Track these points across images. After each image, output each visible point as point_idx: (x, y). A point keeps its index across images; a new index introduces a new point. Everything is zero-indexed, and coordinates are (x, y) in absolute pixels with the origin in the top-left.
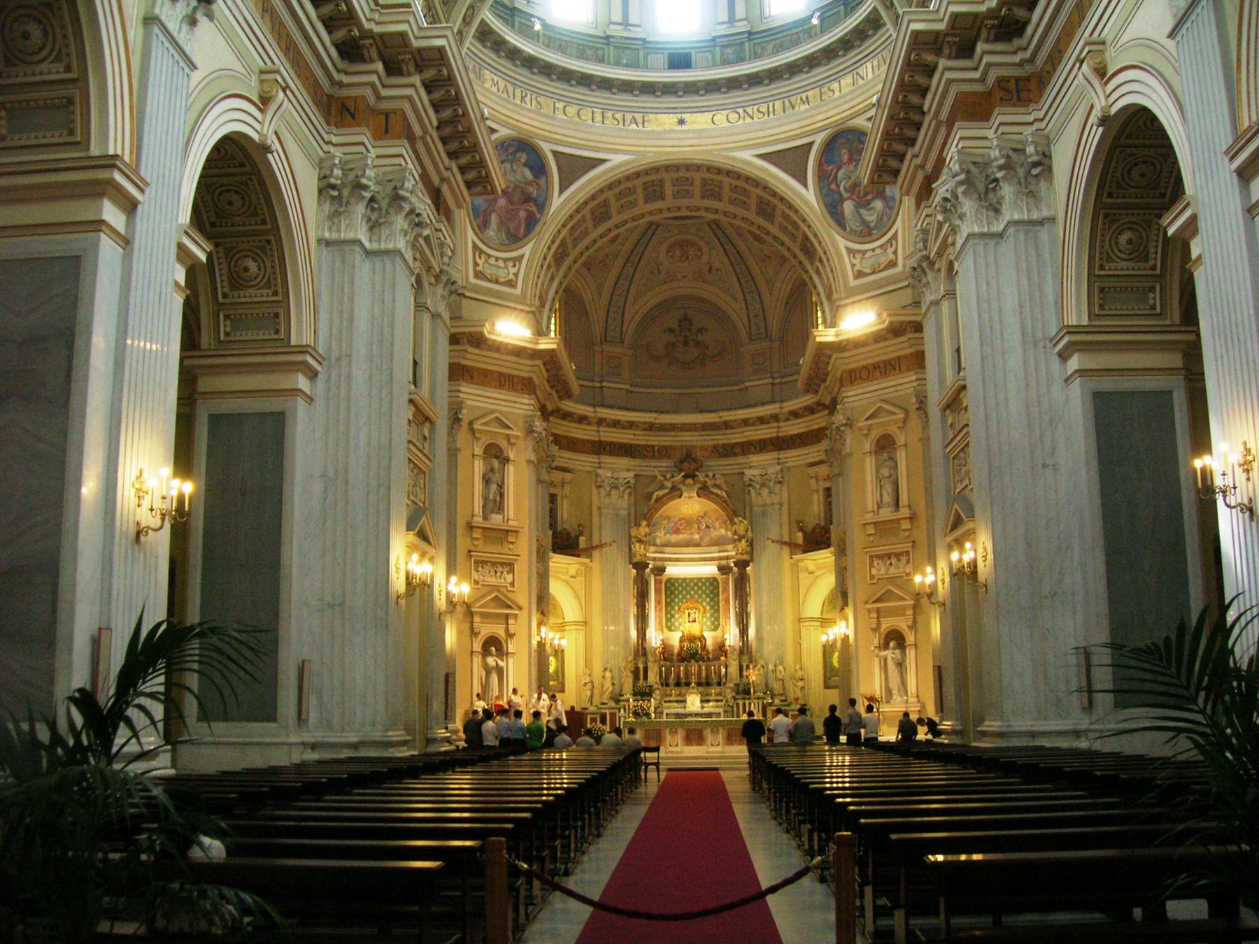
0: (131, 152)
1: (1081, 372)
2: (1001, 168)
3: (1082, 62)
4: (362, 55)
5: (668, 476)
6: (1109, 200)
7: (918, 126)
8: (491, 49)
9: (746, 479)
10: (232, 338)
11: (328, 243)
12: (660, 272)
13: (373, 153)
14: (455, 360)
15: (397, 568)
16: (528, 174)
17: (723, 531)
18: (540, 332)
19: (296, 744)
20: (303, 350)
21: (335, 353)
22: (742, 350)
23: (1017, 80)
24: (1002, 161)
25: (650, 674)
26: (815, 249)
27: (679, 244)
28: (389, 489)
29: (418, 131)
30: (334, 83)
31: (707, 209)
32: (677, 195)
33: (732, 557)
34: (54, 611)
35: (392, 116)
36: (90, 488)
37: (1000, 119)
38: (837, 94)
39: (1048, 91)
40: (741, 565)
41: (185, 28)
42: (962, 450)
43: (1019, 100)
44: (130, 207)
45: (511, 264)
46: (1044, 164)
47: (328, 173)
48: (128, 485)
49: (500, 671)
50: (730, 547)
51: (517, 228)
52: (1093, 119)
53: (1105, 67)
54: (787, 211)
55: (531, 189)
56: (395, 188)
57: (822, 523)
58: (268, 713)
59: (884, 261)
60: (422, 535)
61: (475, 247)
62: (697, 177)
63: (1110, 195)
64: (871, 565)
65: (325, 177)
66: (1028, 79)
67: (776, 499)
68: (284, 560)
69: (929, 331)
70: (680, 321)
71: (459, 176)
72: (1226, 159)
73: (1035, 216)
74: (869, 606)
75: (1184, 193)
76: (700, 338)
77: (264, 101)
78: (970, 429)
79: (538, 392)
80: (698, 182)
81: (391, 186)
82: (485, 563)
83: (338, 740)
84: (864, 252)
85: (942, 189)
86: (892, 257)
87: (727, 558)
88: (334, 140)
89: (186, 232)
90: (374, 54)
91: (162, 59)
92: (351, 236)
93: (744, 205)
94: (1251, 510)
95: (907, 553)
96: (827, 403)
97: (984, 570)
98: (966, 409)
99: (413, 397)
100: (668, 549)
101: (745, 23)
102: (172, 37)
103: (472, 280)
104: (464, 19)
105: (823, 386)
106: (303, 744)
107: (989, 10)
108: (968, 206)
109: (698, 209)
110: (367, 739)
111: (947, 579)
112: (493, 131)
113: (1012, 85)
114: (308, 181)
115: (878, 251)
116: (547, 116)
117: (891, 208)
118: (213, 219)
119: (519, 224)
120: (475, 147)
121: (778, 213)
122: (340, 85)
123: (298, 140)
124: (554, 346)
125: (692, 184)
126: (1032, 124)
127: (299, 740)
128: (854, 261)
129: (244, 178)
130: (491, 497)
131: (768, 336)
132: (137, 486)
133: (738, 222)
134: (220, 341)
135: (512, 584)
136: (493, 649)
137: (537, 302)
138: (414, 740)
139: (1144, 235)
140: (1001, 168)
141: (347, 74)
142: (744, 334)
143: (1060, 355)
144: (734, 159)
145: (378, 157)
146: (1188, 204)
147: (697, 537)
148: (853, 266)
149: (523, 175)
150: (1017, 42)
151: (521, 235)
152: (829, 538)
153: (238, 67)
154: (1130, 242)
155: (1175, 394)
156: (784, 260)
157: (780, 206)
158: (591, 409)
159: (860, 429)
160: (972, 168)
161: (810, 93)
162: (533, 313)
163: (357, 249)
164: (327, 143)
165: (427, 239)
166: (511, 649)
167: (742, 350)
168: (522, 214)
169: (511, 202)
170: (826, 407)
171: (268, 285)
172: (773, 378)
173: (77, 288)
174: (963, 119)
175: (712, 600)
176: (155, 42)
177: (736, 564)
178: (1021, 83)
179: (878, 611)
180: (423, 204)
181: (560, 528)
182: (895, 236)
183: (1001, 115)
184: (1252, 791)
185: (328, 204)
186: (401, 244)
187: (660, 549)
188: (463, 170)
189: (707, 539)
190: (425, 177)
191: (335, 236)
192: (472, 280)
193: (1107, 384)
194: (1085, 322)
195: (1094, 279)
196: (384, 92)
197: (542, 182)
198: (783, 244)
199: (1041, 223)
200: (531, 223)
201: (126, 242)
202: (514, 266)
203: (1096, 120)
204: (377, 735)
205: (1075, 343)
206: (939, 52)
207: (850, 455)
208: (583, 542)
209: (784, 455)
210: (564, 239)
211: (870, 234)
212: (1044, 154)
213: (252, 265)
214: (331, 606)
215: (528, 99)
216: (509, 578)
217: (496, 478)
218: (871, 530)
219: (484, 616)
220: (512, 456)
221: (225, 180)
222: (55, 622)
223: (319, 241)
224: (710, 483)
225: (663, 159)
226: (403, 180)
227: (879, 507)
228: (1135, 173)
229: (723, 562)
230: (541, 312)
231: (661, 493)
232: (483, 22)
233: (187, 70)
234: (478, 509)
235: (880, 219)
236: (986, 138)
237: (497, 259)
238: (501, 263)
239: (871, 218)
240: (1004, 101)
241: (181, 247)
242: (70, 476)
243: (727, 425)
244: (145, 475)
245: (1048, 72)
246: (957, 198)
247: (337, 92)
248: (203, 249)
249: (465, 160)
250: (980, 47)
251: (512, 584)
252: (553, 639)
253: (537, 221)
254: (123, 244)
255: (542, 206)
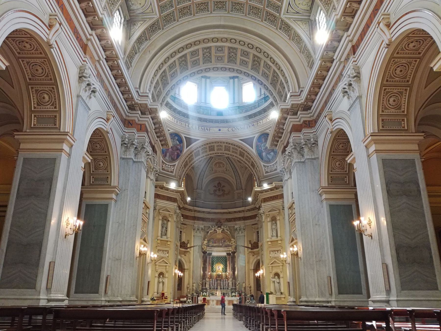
0: (72, 131)
1: (326, 199)
2: (304, 145)
3: (326, 117)
4: (135, 109)
5: (213, 227)
6: (333, 153)
7: (282, 133)
8: (169, 108)
9: (235, 228)
10: (94, 183)
11: (123, 159)
12: (213, 170)
13: (137, 135)
14: (156, 192)
15: (137, 249)
16: (178, 143)
17: (228, 243)
18: (180, 186)
19: (104, 300)
20: (115, 187)
21: (124, 189)
22: (235, 192)
23: (309, 121)
24: (304, 143)
25: (206, 285)
26: (255, 165)
27: (219, 163)
28: (136, 226)
29: (149, 130)
30: (126, 116)
31: (226, 154)
32: (218, 150)
33: (231, 251)
34: (40, 256)
35: (142, 126)
36: (53, 222)
37: (304, 131)
38: (262, 123)
39: (317, 124)
40: (234, 253)
41: (88, 99)
42: (294, 220)
43: (309, 126)
44: (71, 146)
45: (172, 167)
46: (316, 143)
47: (124, 140)
48: (64, 221)
49: (163, 283)
50: (230, 248)
51: (174, 157)
52: (329, 132)
53: (332, 118)
54: (248, 155)
55: (178, 147)
56: (143, 145)
57: (256, 242)
58: (96, 291)
59: (274, 169)
60: (145, 240)
61: (162, 162)
62: (224, 145)
63: (333, 152)
64: (270, 254)
65: (123, 141)
66: (312, 121)
67: (243, 234)
68: (105, 246)
69: (285, 188)
70: (218, 184)
71: (159, 142)
72: (362, 143)
73: (313, 157)
74: (269, 265)
75: (351, 151)
76: (223, 188)
77: (108, 120)
78: (296, 214)
79: (178, 202)
80: (224, 146)
81: (142, 144)
82: (161, 250)
83: (116, 299)
84: (268, 166)
85: (288, 149)
86: (275, 168)
87: (229, 251)
88: (126, 131)
89: (85, 154)
90: (138, 109)
91: (81, 109)
92: (129, 157)
93: (236, 153)
94: (371, 236)
95: (280, 250)
96: (258, 207)
97: (300, 254)
98: (294, 209)
99: (145, 201)
100: (213, 248)
101: (238, 104)
102: (84, 101)
103: (161, 170)
104: (162, 100)
105: (257, 202)
106: (106, 300)
107: (302, 103)
108: (295, 154)
109: (224, 153)
110: (125, 299)
111: (290, 256)
112: (169, 130)
113: (308, 123)
114: (119, 141)
115: (272, 166)
116: (184, 127)
117: (275, 155)
118: (91, 150)
119: (175, 156)
120: (164, 135)
121: (245, 155)
122: (129, 116)
123: (117, 131)
124: (183, 190)
125: (222, 147)
126: (313, 133)
127: (104, 299)
128: (265, 169)
129: (101, 140)
130: (164, 231)
131: (242, 188)
132: (67, 222)
133: (234, 157)
134: (91, 184)
135: (168, 257)
136: (161, 276)
137: (179, 177)
138: (138, 300)
139: (343, 162)
140: (304, 145)
141: (130, 113)
142: (235, 188)
143: (320, 194)
144: (234, 141)
145: (138, 136)
146: (353, 155)
147: (221, 244)
148: (265, 170)
149: (176, 142)
150: (309, 111)
151: (175, 159)
152: (258, 246)
153: (102, 111)
154: (339, 164)
155: (353, 206)
156: (246, 168)
157: (246, 154)
158: (192, 207)
159: (267, 215)
160: (296, 144)
161: (254, 123)
162: (178, 180)
163: (131, 160)
164: (124, 132)
165: (150, 159)
166: (167, 276)
167: (235, 192)
168: (176, 153)
169: (173, 150)
170: (257, 208)
171: (106, 169)
172: (243, 200)
173: (54, 166)
174: (294, 132)
175: (225, 263)
176: (79, 102)
177: (232, 252)
178: (310, 122)
179: (272, 266)
180: (150, 149)
181: (182, 241)
182: (277, 162)
183: (304, 130)
184: (179, 1)
185: (124, 148)
186: (143, 160)
187: (211, 248)
188: (161, 141)
189: (224, 245)
190: (150, 142)
191: (125, 157)
192: (161, 170)
193: (333, 202)
194: (327, 185)
195: (329, 174)
196: (140, 119)
197: (181, 145)
198: (246, 164)
199: (315, 159)
200: (178, 156)
201: (69, 155)
202: (173, 167)
203: (329, 132)
204: (128, 299)
205: (324, 191)
206: (288, 114)
207: (264, 222)
208: (188, 246)
209: (246, 221)
210: (187, 160)
211: (270, 162)
212: (316, 141)
213: (101, 163)
214: (117, 260)
215: (178, 122)
216: (167, 255)
217: (165, 226)
218: (270, 243)
219: (159, 266)
220: (170, 220)
221: (95, 140)
222: (39, 259)
223: (121, 158)
224: (225, 229)
225: (214, 140)
226: (145, 143)
227: (272, 237)
228: (341, 146)
229: (228, 252)
230: (180, 180)
231: (211, 231)
232: (167, 101)
233: (88, 110)
234: (159, 234)
235: (273, 157)
236: (300, 137)
237: (168, 165)
238: (169, 166)
239: (270, 157)
240: (305, 127)
241: (84, 157)
242: (48, 218)
243: (230, 213)
244: (69, 219)
245: (317, 119)
246: (292, 152)
247: (128, 118)
248: (90, 159)
249: (161, 138)
250: (299, 113)
251: (168, 257)
252: (179, 273)
253: (180, 155)
254: (68, 156)
255: (181, 151)
